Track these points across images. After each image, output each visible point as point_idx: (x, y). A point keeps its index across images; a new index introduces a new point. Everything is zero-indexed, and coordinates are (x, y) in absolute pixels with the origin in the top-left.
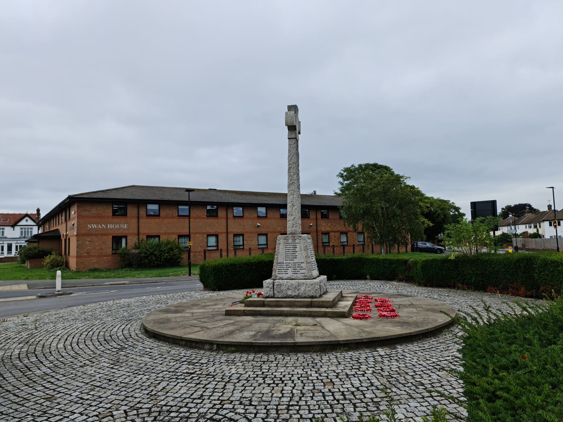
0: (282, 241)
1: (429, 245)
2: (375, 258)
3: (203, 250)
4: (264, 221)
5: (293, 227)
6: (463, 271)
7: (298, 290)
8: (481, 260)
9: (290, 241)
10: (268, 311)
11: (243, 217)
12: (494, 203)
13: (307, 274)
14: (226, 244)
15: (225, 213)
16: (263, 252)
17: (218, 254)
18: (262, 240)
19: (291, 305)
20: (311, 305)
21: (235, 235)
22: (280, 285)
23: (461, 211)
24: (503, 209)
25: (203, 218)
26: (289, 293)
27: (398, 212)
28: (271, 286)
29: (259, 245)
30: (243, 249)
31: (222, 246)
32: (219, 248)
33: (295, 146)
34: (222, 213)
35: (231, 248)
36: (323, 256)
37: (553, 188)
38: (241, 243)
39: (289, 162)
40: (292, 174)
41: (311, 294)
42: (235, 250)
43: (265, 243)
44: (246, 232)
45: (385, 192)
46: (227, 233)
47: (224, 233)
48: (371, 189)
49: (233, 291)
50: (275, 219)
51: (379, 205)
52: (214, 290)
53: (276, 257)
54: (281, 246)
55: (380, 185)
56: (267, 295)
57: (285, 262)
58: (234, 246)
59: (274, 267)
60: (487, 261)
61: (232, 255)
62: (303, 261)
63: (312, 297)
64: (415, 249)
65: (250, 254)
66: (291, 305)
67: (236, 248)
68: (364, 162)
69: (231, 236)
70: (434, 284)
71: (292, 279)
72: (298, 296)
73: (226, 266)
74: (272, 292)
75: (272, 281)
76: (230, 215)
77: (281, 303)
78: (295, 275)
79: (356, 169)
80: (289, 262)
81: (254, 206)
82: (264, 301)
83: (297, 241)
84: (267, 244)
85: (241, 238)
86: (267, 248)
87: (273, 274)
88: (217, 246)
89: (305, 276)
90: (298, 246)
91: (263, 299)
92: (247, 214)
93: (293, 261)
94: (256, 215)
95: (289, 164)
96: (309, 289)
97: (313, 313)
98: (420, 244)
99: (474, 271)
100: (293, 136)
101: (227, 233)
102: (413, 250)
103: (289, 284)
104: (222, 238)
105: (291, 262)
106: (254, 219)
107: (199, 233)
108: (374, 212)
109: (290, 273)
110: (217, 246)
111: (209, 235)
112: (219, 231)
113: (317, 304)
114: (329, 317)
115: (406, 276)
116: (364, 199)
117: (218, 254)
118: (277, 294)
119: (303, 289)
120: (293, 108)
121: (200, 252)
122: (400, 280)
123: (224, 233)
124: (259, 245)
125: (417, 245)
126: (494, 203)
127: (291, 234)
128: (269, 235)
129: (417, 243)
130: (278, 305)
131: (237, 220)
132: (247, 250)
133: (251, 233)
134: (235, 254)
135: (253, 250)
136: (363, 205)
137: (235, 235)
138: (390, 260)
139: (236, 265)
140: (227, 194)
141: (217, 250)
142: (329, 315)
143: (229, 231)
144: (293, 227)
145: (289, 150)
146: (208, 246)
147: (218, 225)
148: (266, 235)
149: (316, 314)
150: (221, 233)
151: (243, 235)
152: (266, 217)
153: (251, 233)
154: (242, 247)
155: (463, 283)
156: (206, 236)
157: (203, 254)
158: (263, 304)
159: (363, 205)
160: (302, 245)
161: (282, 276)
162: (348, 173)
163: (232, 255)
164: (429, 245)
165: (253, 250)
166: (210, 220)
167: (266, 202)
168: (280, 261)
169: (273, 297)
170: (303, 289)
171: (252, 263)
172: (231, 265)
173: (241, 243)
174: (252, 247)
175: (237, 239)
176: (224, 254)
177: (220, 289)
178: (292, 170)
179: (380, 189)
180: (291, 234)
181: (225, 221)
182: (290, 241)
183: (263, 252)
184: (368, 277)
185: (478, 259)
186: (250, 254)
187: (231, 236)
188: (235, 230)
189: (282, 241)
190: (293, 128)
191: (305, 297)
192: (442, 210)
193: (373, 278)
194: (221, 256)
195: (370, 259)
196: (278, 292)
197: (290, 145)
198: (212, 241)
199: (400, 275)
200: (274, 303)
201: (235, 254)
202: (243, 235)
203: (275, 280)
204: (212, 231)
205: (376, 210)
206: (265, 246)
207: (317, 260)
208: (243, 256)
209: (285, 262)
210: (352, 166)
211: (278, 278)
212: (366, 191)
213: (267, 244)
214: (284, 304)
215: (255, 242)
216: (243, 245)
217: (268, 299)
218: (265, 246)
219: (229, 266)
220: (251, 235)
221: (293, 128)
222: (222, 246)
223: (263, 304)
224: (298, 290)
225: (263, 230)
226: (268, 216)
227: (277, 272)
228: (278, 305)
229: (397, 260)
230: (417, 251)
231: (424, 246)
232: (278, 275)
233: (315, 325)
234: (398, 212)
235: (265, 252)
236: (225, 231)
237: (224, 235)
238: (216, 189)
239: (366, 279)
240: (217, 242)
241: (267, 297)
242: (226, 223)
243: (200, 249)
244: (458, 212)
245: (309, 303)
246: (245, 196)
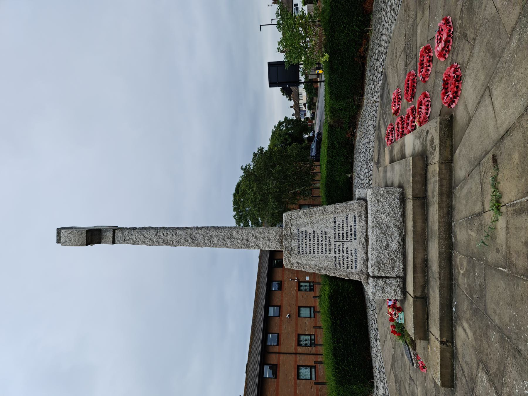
0: (294, 260)
1: (313, 146)
2: (326, 166)
3: (315, 386)
4: (284, 309)
5: (269, 239)
6: (345, 43)
7: (388, 227)
8: (330, 17)
9: (294, 243)
10: (441, 288)
11: (278, 334)
12: (270, 64)
13: (356, 213)
14: (309, 356)
15: (273, 356)
16: (319, 312)
17: (319, 366)
18: (305, 312)
19: (422, 240)
20: (422, 200)
21: (299, 344)
22: (379, 264)
23: (282, 120)
24: (283, 95)
25: (278, 382)
26: (394, 245)
27: (278, 168)
28: (380, 282)
29: (310, 317)
30: (314, 335)
31: (310, 360)
32: (314, 365)
33: (126, 232)
34: (273, 359)
35: (313, 350)
36: (323, 199)
37: (261, 25)
38: (308, 337)
39: (153, 244)
40: (175, 237)
41: (396, 202)
42: (316, 345)
43: (308, 309)
44: (296, 331)
45: (258, 180)
46: (296, 354)
47: (296, 358)
48: (255, 194)
49: (373, 355)
50: (282, 296)
51: (273, 185)
52: (372, 385)
53: (323, 272)
54: (304, 261)
55: (250, 185)
56: (399, 291)
57: (333, 254)
58: (311, 346)
59: (344, 276)
60: (332, 7)
61: (321, 350)
62: (332, 220)
63: (403, 200)
64: (317, 158)
65: (320, 327)
66: (422, 240)
67: (314, 344)
68: (231, 207)
69: (300, 349)
70: (360, 84)
71: (367, 240)
72: (402, 229)
73: (337, 363)
74: (394, 281)
75: (370, 280)
76: (276, 349)
77: (419, 261)
78: (359, 234)
79: (238, 213)
80: (332, 247)
81: (267, 319)
82: (415, 298)
83: (296, 231)
84: (310, 307)
85: (302, 337)
86: (314, 307)
87: (356, 278)
88: (311, 367)
89: (361, 215)
90: (303, 229)
91: (410, 300)
92: (275, 329)
93: (332, 240)
94: (278, 318)
95: (158, 243)
96: (386, 205)
97: (445, 189)
98: (313, 153)
99: (345, 27)
100: (110, 234)
101: (296, 354)
102: (318, 160)
103: (377, 246)
104: (301, 360)
105: (333, 243)
106: (281, 321)
107: (295, 389)
108: (278, 190)
109: (355, 245)
110: (311, 367)
111: (298, 377)
112: (293, 363)
113: (419, 186)
114: (452, 154)
115: (349, 127)
116: (264, 201)
117: (319, 366)
118: (398, 271)
119: (386, 219)
120: (62, 235)
121: (317, 390)
122: (354, 135)
123: (296, 358)
124: (310, 317)
125: (313, 156)
126: (270, 64)
127: (281, 243)
128: (300, 305)
129: (312, 156)
130: (423, 268)
131: (282, 341)
132: (316, 331)
133: (297, 325)
134: (321, 345)
135: (316, 323)
136: (271, 201)
137: (299, 344)
138: (329, 148)
139: (335, 348)
140: (253, 351)
141: (315, 367)
142: (447, 153)
143: (294, 351)
144: (269, 239)
145: (133, 243)
146: (311, 379)
147: (287, 365)
148: (299, 308)
149: (445, 182)
150: (296, 361)
151: (299, 335)
152: (280, 306)
153: (297, 325)
154: (313, 337)
155: (361, 45)
156: (298, 380)
157: (320, 386)
158: (422, 301)
159: (271, 201)
160: (301, 221)
161: (360, 261)
162: (241, 222)
163: (321, 350)
164: (313, 146)
165: (316, 323)
166: (281, 374)
167: (264, 306)
168: (331, 265)
169: (404, 280)
170: (386, 219)
171: (333, 324)
172: (335, 355)
173: (308, 337)
174: (313, 325)
175: (303, 342)
176: (320, 359)
177: (370, 376)
178: (169, 239)
179: (254, 185)
180: (281, 243)
181: (282, 356)
182: (294, 243)
183: (319, 312)
184: (350, 175)
185: (329, 21)
186: (320, 327)
187: (300, 349)
188: (293, 344)
189: (294, 260)
190: (93, 236)
191: (404, 215)
192: (280, 136)
193: (351, 169)
194: (321, 363)
195: (327, 172)
196: (393, 268)
197: (125, 242)
198: (305, 372)
199: (347, 136)
200: (419, 275)
201: (321, 345)
202: (299, 335)
203: (368, 276)
204: (293, 373)
205: (276, 188)
206: (312, 309)
207: (329, 203)
208: (323, 336)
209: (333, 254)
210: (234, 217)
211: (364, 269)
212: (256, 198)
213: (310, 307)
214: (420, 256)
215: (307, 321)
216: (310, 335)
217: (410, 288)
218: (312, 309)
219: (336, 358)
220: (299, 325)
221: (93, 236)
222: (310, 360)
223: (422, 301)
224: (388, 227)
225: (295, 311)
226: (279, 304)
227: (353, 271)
228: (423, 268)
229: (328, 139)
230: (319, 156)
231: (314, 150)
232: (358, 269)
233: (495, 160)
234: (278, 168)
235: (318, 309)
236: (294, 356)
237: (299, 357)
238: (247, 365)
239: (352, 178)
240: (306, 366)
241: (404, 291)
242: (285, 355)
243: (314, 390)
244: (283, 122)
245: (418, 203)
246: (256, 331)
